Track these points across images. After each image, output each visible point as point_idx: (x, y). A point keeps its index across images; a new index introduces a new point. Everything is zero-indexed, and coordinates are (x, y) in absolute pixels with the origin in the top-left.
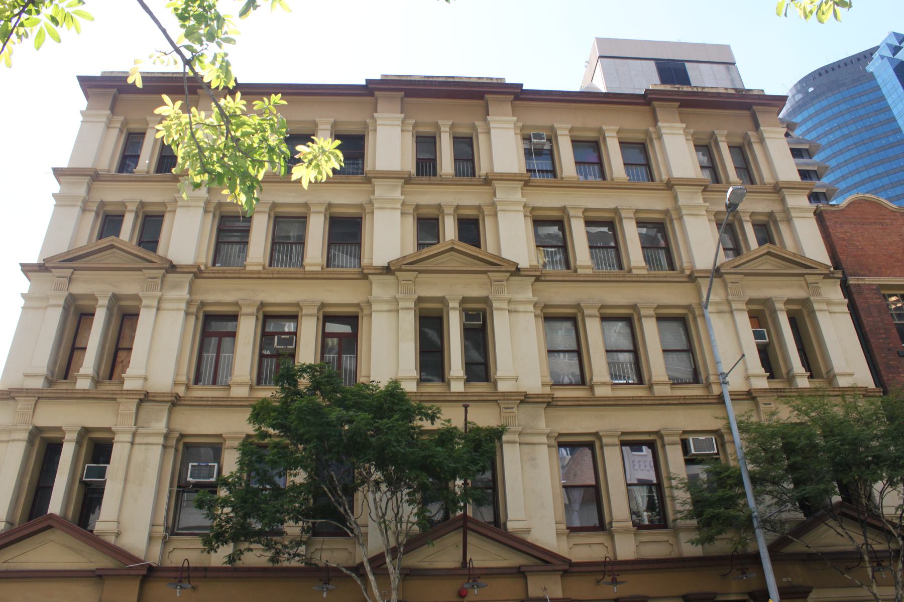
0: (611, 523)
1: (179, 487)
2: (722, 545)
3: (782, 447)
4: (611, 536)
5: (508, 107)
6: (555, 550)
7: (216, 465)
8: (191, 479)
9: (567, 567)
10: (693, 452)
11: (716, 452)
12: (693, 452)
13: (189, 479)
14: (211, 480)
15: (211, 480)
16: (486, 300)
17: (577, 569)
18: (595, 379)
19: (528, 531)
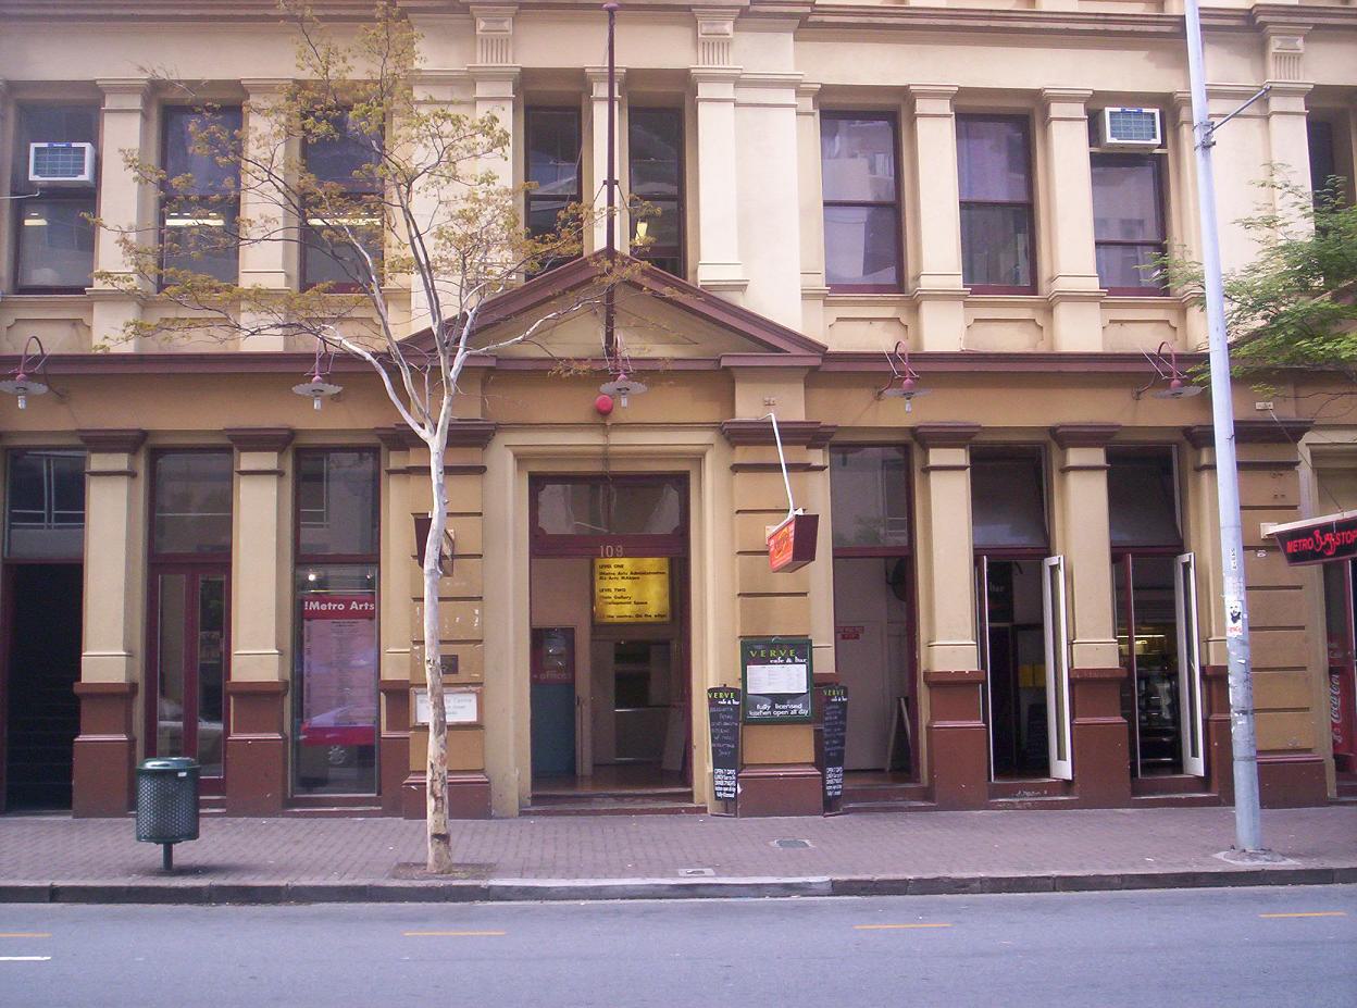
0: (917, 278)
1: (13, 193)
2: (1143, 335)
3: (1337, 546)
4: (914, 306)
5: (801, 387)
6: (797, 326)
7: (88, 146)
8: (37, 178)
9: (817, 362)
10: (1110, 140)
11: (1158, 141)
12: (1110, 140)
13: (32, 177)
14: (80, 178)
15: (80, 178)
16: (689, 472)
17: (838, 367)
18: (926, 283)
19: (741, 287)
